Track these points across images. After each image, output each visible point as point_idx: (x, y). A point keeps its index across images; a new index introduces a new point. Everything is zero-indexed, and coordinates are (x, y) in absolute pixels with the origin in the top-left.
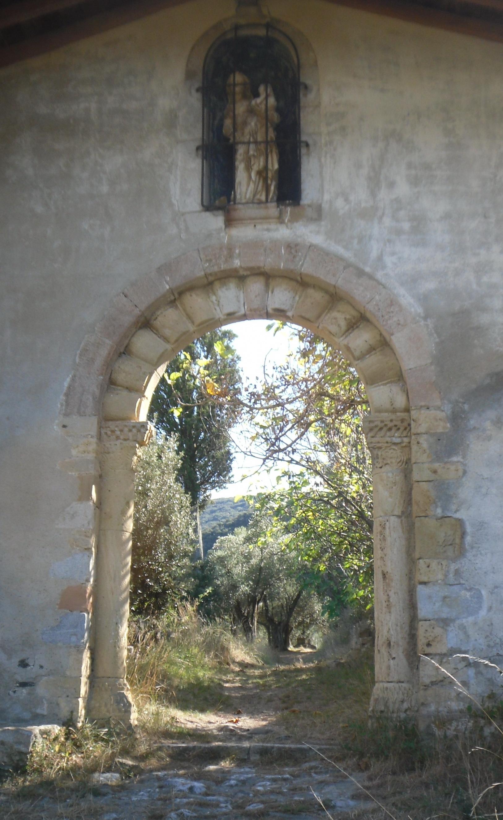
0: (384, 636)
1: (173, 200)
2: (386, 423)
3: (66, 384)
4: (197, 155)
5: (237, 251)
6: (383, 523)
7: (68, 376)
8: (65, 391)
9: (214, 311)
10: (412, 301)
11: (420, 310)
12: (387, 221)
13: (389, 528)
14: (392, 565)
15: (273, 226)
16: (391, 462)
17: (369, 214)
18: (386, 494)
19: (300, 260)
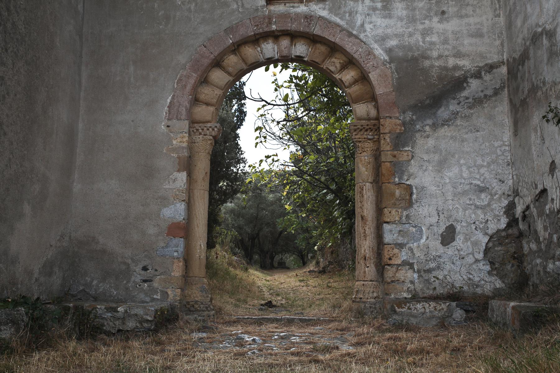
3: (169, 101)
5: (274, 20)
10: (382, 52)
11: (387, 58)
19: (313, 26)
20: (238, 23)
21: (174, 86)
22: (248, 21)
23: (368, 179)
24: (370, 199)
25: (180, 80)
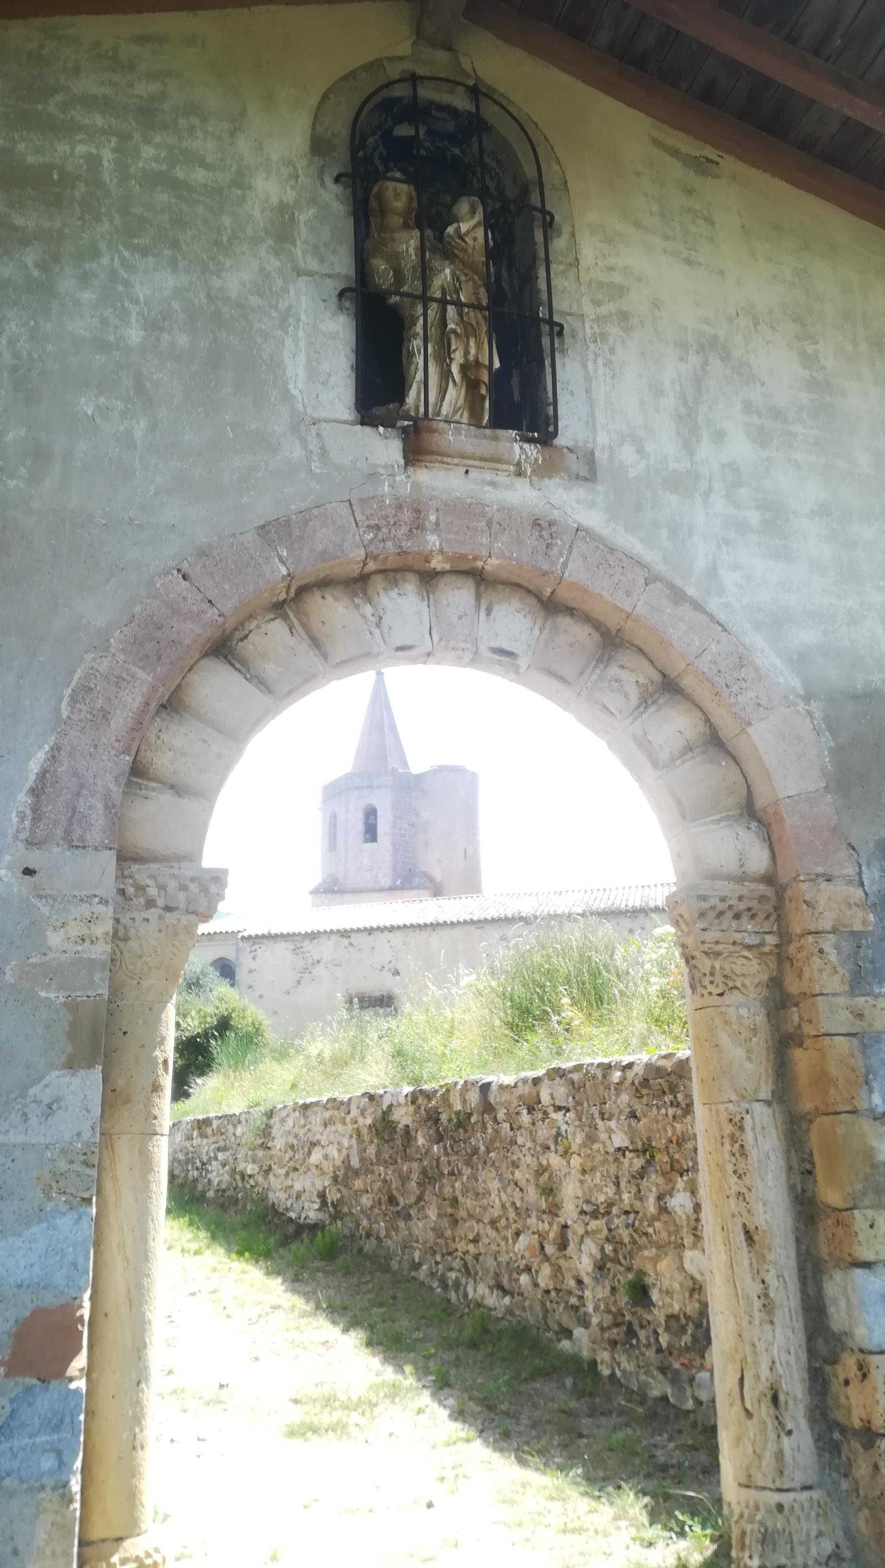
0: (763, 1379)
1: (291, 386)
2: (731, 902)
3: (34, 766)
4: (341, 308)
5: (433, 518)
6: (738, 1118)
7: (40, 747)
8: (30, 783)
9: (368, 636)
10: (778, 662)
11: (795, 682)
12: (718, 503)
13: (753, 1129)
14: (765, 1212)
15: (502, 478)
16: (744, 985)
17: (683, 483)
18: (739, 1053)
19: (561, 554)
20: (308, 510)
21: (58, 709)
22: (344, 509)
23: (756, 1091)
24: (772, 1165)
25: (85, 690)
